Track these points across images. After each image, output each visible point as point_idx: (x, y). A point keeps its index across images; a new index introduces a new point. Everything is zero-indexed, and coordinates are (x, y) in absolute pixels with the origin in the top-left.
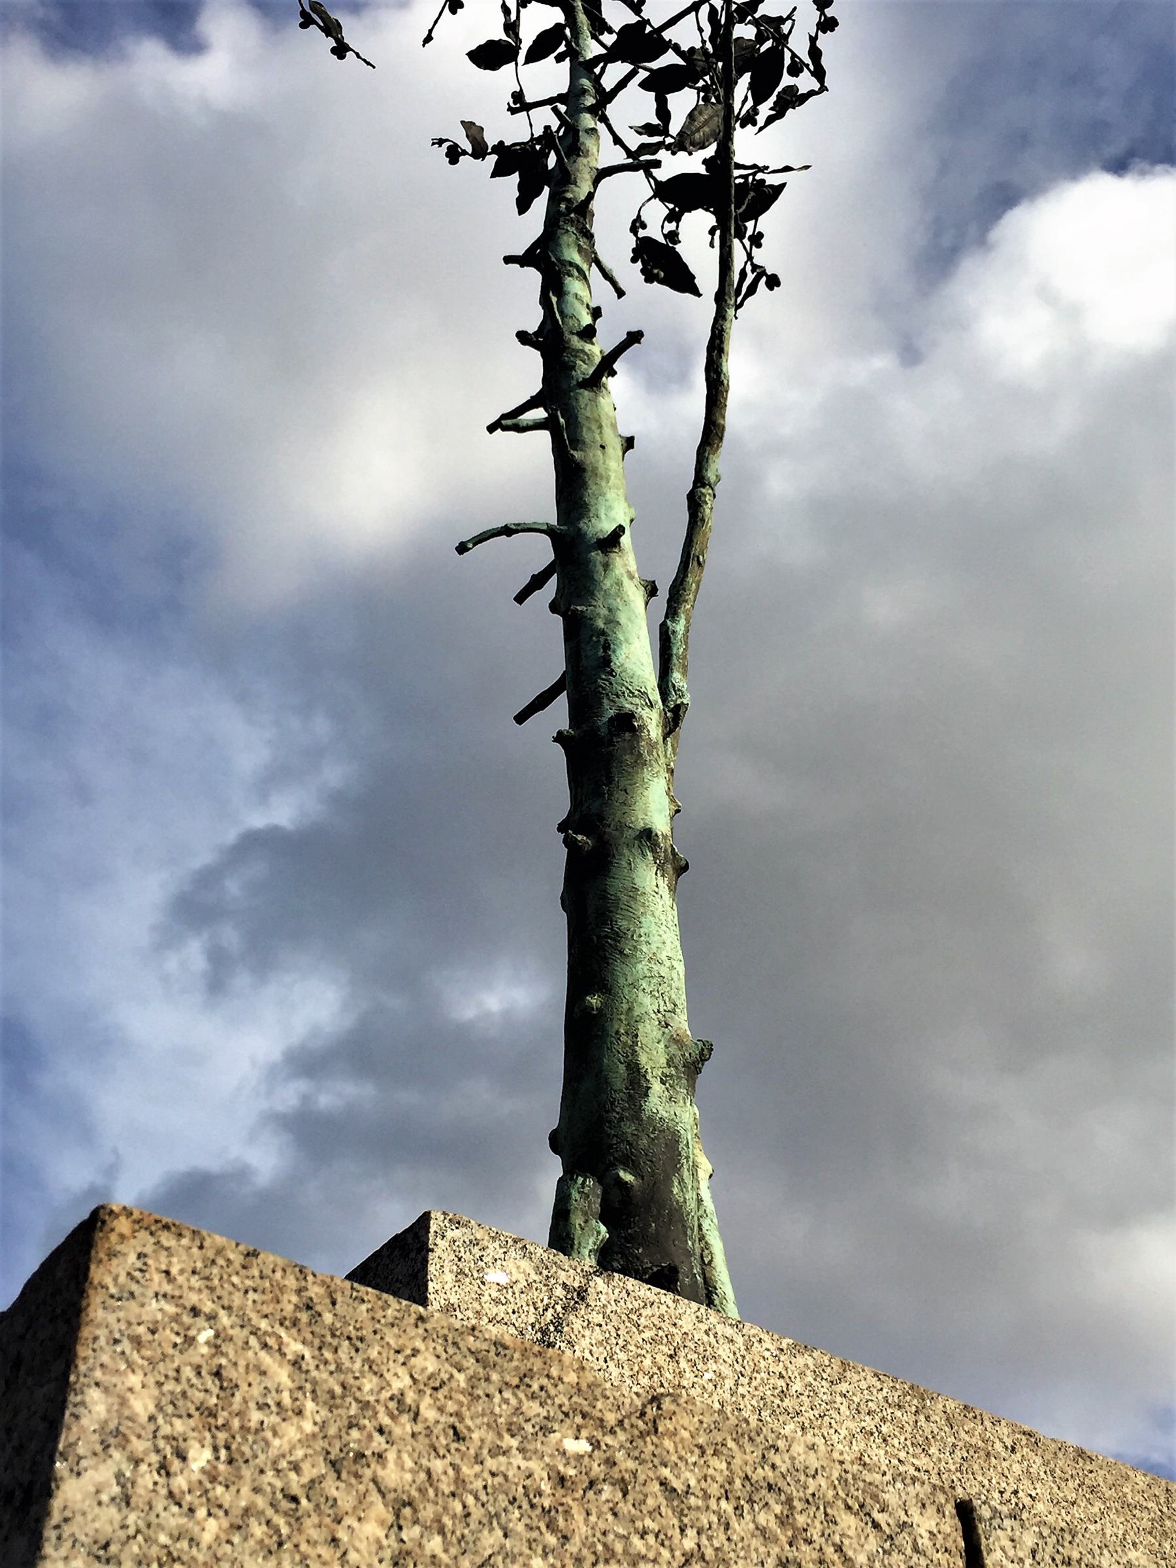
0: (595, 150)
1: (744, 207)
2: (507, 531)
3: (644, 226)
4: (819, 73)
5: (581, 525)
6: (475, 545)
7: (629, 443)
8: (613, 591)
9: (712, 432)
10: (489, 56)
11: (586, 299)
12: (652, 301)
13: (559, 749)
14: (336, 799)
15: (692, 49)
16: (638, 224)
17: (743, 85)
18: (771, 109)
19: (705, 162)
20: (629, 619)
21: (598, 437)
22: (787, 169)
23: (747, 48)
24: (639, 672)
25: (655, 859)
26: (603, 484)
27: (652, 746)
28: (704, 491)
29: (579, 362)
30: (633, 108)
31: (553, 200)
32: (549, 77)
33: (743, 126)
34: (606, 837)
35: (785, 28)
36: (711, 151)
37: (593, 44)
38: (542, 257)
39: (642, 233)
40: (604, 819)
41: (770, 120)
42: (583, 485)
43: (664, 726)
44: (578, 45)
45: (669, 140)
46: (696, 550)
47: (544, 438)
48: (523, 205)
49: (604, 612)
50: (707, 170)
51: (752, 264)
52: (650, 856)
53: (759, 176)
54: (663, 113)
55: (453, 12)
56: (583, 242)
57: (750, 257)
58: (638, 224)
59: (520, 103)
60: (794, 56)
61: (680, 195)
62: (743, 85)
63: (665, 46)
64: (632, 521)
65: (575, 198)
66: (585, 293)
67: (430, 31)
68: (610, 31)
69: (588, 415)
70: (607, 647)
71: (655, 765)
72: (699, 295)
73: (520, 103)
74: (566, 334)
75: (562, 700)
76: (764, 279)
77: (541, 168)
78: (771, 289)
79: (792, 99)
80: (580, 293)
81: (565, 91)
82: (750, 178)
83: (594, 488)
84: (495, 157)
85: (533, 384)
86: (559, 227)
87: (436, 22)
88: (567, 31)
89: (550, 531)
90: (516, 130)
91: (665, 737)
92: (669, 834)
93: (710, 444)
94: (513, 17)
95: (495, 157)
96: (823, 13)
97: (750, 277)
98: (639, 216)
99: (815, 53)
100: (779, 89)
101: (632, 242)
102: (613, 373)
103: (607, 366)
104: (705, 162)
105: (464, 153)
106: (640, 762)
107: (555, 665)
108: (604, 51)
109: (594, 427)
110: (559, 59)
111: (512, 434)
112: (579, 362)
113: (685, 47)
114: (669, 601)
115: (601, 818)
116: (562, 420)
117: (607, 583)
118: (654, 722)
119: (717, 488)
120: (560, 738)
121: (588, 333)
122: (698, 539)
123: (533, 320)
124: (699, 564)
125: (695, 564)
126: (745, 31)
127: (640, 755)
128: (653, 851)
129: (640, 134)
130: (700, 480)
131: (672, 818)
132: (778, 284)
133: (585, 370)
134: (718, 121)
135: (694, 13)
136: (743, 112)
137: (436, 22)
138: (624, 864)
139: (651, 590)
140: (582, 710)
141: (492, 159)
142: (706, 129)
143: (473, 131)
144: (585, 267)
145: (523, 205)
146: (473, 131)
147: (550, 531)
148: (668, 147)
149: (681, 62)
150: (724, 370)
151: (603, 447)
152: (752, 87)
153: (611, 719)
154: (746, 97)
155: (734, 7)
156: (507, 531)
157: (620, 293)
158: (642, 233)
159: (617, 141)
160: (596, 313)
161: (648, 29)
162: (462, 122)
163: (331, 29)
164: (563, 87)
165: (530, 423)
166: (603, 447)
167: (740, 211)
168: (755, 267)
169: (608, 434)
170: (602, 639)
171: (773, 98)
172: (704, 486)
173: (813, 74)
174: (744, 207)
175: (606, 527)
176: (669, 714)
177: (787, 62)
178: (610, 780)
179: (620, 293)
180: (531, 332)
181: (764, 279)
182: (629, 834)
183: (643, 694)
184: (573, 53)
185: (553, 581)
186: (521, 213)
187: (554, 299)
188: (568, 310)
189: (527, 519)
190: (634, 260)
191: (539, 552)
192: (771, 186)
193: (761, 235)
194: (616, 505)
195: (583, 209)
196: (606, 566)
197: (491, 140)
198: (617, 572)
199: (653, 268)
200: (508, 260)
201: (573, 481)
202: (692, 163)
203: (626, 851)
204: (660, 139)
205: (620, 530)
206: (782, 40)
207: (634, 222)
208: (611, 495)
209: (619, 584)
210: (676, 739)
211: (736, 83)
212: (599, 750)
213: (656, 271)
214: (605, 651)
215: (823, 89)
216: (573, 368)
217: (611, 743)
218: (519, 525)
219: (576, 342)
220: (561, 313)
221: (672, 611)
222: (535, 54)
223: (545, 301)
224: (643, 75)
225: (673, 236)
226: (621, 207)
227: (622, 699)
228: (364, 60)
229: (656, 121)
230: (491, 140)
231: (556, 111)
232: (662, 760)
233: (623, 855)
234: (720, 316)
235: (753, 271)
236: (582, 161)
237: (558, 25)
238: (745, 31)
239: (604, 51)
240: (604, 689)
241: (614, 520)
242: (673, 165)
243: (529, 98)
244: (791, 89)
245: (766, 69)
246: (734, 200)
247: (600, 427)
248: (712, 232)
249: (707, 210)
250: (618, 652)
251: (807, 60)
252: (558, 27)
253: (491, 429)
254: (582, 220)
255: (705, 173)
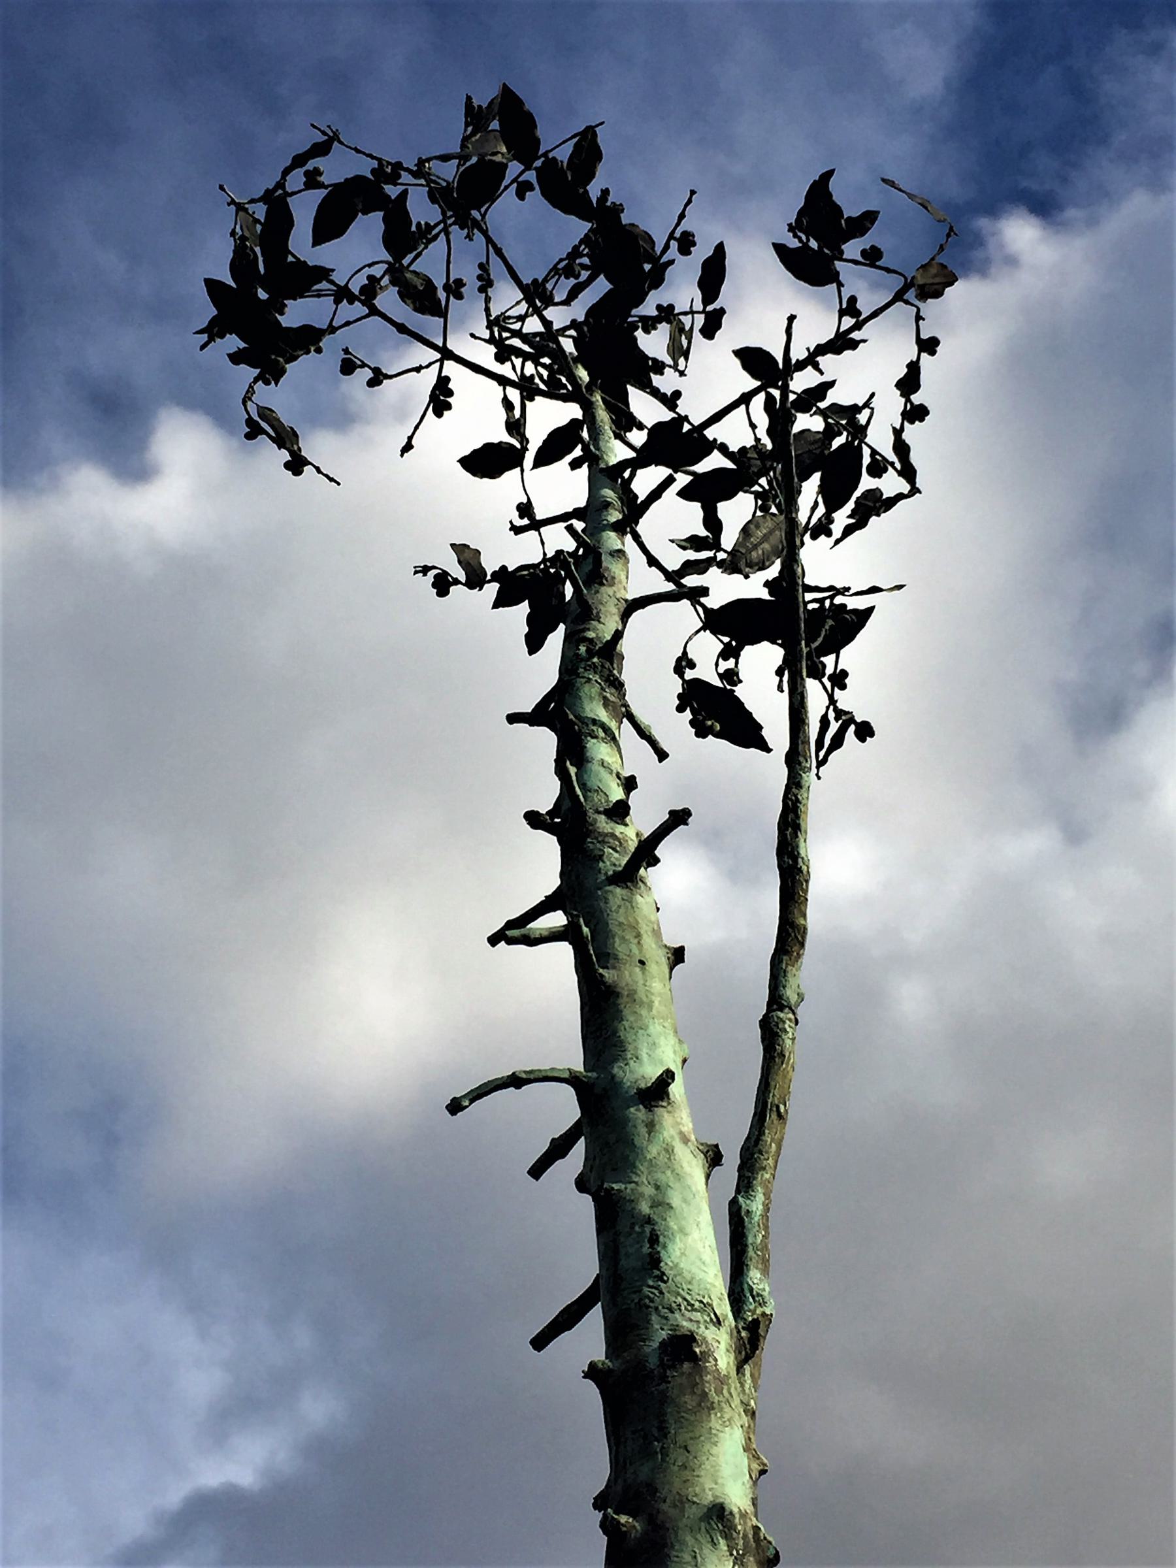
0: (623, 577)
1: (820, 640)
2: (516, 1081)
3: (692, 665)
4: (908, 473)
5: (615, 1070)
6: (472, 1101)
7: (678, 955)
8: (663, 1158)
9: (790, 937)
10: (487, 462)
11: (616, 767)
12: (706, 764)
13: (591, 1390)
14: (319, 1449)
15: (743, 450)
16: (683, 663)
17: (810, 488)
18: (849, 517)
19: (767, 584)
20: (685, 1201)
21: (635, 950)
22: (874, 590)
23: (815, 442)
24: (701, 1275)
25: (730, 1550)
26: (644, 1012)
27: (722, 1380)
28: (781, 1015)
29: (608, 850)
30: (672, 520)
31: (571, 640)
32: (562, 487)
33: (814, 537)
34: (661, 1517)
35: (862, 418)
36: (773, 571)
37: (617, 445)
38: (556, 712)
39: (689, 674)
40: (656, 1490)
41: (848, 531)
42: (618, 1016)
43: (738, 1351)
44: (598, 449)
45: (721, 556)
46: (773, 1098)
47: (564, 952)
48: (534, 643)
49: (649, 1191)
50: (771, 594)
51: (836, 710)
52: (723, 1544)
53: (839, 600)
54: (713, 523)
55: (439, 414)
56: (610, 694)
57: (832, 701)
58: (683, 663)
59: (528, 518)
60: (874, 452)
61: (737, 625)
62: (810, 488)
63: (709, 446)
64: (684, 1061)
65: (598, 638)
66: (617, 757)
67: (410, 438)
68: (641, 427)
69: (622, 919)
70: (654, 1240)
71: (727, 1409)
72: (769, 750)
73: (528, 518)
74: (590, 813)
75: (595, 1318)
76: (852, 728)
77: (557, 596)
78: (863, 740)
79: (874, 505)
80: (608, 759)
81: (582, 503)
82: (827, 603)
83: (632, 1019)
84: (495, 586)
85: (549, 880)
86: (578, 676)
87: (417, 427)
88: (585, 434)
89: (573, 1080)
90: (526, 551)
91: (739, 1369)
92: (750, 1509)
93: (787, 953)
94: (517, 413)
95: (495, 586)
96: (908, 400)
97: (834, 727)
98: (685, 653)
99: (901, 448)
100: (857, 493)
101: (677, 686)
102: (655, 861)
103: (646, 853)
104: (767, 584)
105: (456, 582)
106: (705, 1405)
107: (584, 1267)
108: (632, 454)
109: (629, 936)
110: (575, 465)
111: (522, 948)
112: (608, 850)
113: (734, 447)
114: (740, 1169)
115: (652, 1489)
116: (586, 930)
117: (653, 1150)
118: (723, 1346)
119: (799, 1011)
120: (593, 1372)
121: (620, 812)
122: (777, 1081)
123: (545, 794)
124: (780, 1116)
125: (774, 1116)
126: (808, 422)
127: (705, 1395)
128: (727, 1537)
129: (684, 548)
130: (776, 1001)
131: (755, 1483)
132: (872, 734)
133: (616, 860)
134: (779, 535)
135: (743, 407)
136: (814, 521)
137: (417, 427)
138: (687, 1557)
139: (714, 1157)
140: (619, 1333)
141: (492, 589)
142: (766, 546)
143: (467, 555)
144: (613, 725)
145: (534, 643)
146: (467, 555)
147: (573, 1080)
148: (720, 564)
149: (730, 465)
150: (802, 852)
151: (642, 963)
152: (823, 489)
153: (663, 1344)
154: (816, 504)
155: (792, 397)
156: (516, 1081)
157: (662, 755)
158: (689, 674)
159: (653, 561)
160: (630, 784)
161: (686, 427)
162: (453, 545)
163: (285, 438)
164: (580, 499)
165: (545, 933)
166: (642, 963)
167: (814, 646)
168: (839, 713)
169: (648, 941)
170: (648, 1229)
171: (850, 505)
172: (781, 1008)
173: (900, 473)
174: (820, 640)
175: (650, 1072)
176: (744, 1334)
177: (866, 460)
178: (663, 1432)
179: (662, 755)
180: (543, 812)
181: (852, 728)
182: (692, 1512)
183: (706, 1307)
184: (591, 458)
185: (580, 1147)
186: (531, 652)
187: (573, 770)
188: (593, 783)
189: (543, 1065)
190: (680, 709)
191: (561, 1108)
192: (855, 611)
193: (844, 674)
194: (662, 1041)
195: (610, 651)
196: (651, 1126)
197: (490, 565)
198: (665, 1134)
199: (705, 719)
200: (513, 718)
201: (604, 1011)
202: (753, 587)
203: (689, 1539)
204: (710, 554)
205: (667, 1077)
206: (859, 432)
207: (679, 660)
208: (655, 1028)
209: (669, 1151)
210: (758, 1366)
211: (799, 492)
212: (649, 1391)
213: (709, 723)
214: (651, 1247)
215: (914, 490)
216: (601, 858)
217: (664, 1379)
218: (531, 1072)
219: (604, 824)
220: (583, 786)
221: (745, 1184)
222: (546, 457)
223: (561, 771)
224: (682, 480)
225: (731, 677)
226: (658, 647)
227: (677, 1315)
228: (327, 476)
229: (703, 532)
230: (490, 565)
231: (570, 529)
232: (736, 1402)
233: (684, 1543)
234: (794, 783)
235: (837, 719)
236: (606, 591)
237: (574, 421)
238: (808, 422)
239: (632, 454)
240: (652, 1301)
241: (661, 1062)
242: (724, 588)
243: (540, 515)
244: (874, 494)
245: (841, 469)
246: (810, 630)
247: (638, 936)
248: (779, 672)
249: (773, 642)
250: (670, 1247)
251: (892, 457)
252: (574, 424)
253: (494, 940)
254: (608, 665)
255: (768, 597)
